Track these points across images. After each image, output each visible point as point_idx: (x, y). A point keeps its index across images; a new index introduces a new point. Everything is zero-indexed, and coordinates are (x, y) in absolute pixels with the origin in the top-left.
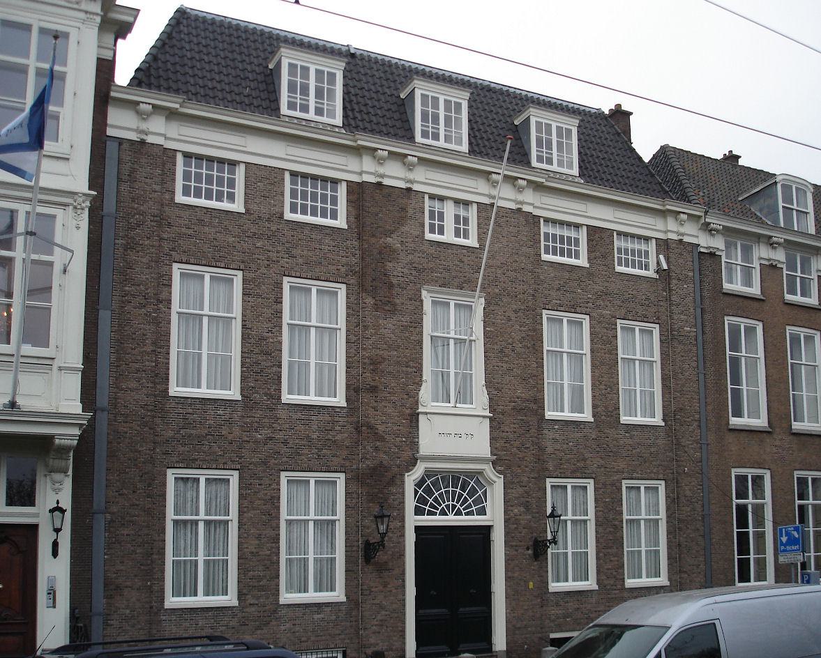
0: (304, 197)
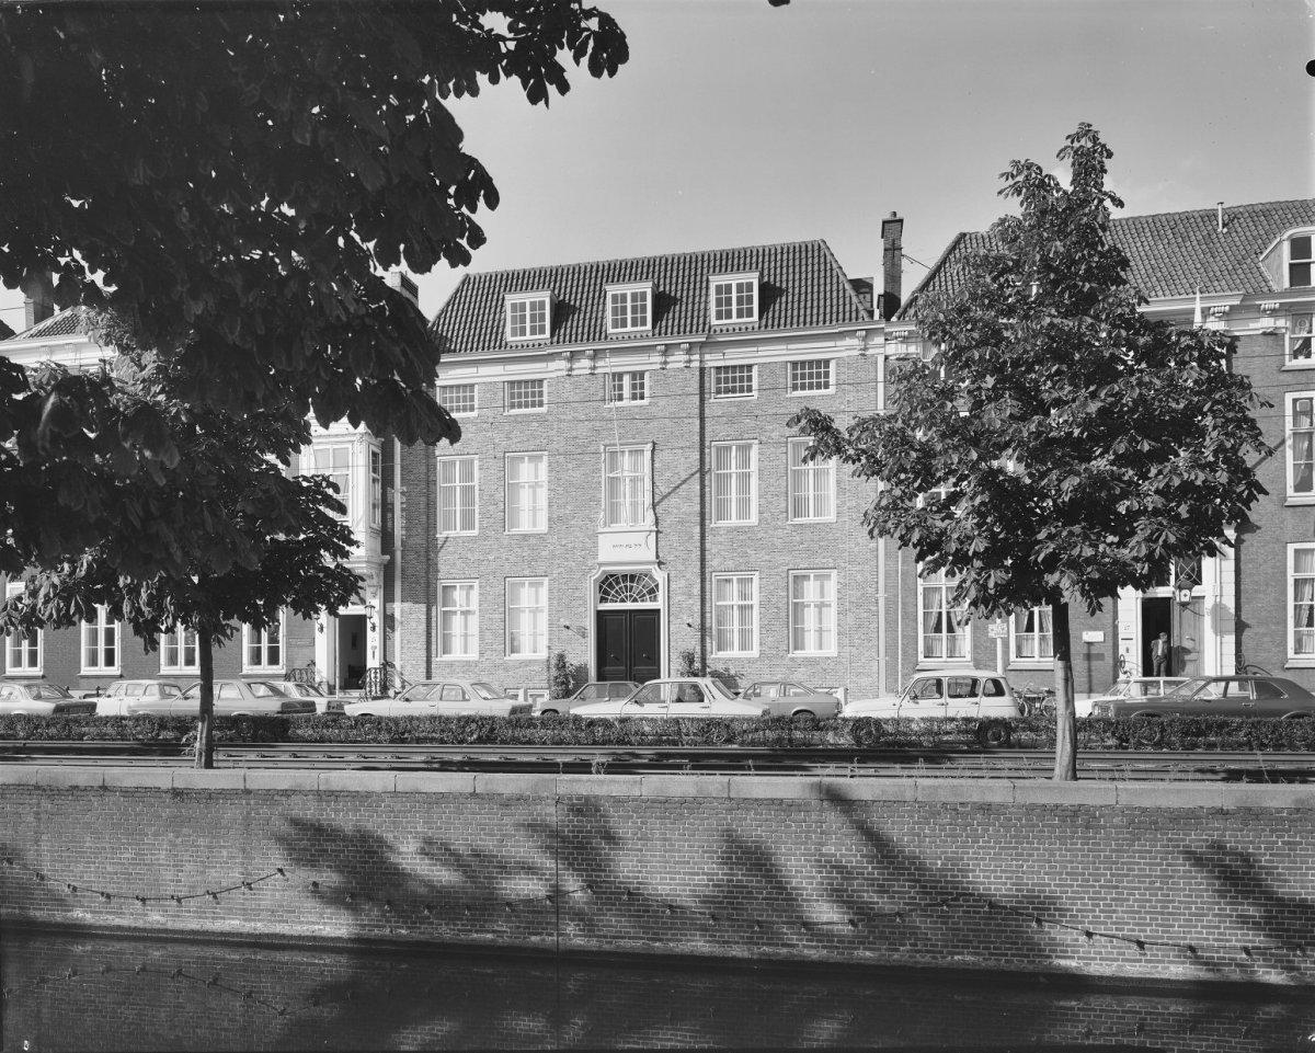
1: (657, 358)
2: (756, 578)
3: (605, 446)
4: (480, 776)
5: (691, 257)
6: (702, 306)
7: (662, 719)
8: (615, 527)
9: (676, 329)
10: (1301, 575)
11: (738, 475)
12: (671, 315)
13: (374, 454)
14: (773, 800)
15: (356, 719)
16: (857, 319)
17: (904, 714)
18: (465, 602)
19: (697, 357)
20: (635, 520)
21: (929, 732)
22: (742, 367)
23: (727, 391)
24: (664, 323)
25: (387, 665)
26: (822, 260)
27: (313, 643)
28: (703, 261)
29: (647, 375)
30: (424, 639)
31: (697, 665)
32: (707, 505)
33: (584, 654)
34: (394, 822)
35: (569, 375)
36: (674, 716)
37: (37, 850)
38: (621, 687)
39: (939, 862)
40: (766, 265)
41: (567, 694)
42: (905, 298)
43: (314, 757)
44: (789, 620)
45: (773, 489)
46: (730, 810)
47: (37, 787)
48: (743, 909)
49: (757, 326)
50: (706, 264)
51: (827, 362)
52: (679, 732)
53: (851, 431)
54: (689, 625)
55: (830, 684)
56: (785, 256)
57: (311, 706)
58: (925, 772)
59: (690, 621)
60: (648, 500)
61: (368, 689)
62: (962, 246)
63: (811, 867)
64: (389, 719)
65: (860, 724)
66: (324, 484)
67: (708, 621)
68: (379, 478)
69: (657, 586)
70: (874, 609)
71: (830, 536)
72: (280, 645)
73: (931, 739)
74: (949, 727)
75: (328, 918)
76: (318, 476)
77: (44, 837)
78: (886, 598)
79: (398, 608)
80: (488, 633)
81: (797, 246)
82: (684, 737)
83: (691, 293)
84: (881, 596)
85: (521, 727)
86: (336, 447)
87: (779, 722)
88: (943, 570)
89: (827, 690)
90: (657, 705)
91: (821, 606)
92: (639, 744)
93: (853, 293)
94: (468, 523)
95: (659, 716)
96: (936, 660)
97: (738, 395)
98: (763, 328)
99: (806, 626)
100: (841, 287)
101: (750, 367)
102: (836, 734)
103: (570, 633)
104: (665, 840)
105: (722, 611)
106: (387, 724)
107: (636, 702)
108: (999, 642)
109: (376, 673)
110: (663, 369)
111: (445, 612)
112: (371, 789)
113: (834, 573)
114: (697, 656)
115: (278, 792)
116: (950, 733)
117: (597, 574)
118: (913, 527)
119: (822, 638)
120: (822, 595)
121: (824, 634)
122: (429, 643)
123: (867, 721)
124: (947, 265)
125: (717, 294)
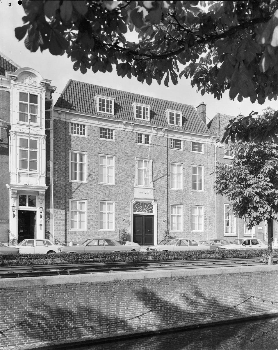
0: (174, 144)
8: (140, 186)
19: (166, 134)
35: (124, 130)
37: (261, 292)
44: (189, 220)
47: (261, 272)
77: (263, 288)
78: (217, 216)
79: (52, 210)
80: (91, 221)
86: (31, 139)
91: (109, 214)
110: (156, 135)
117: (134, 202)
122: (66, 224)
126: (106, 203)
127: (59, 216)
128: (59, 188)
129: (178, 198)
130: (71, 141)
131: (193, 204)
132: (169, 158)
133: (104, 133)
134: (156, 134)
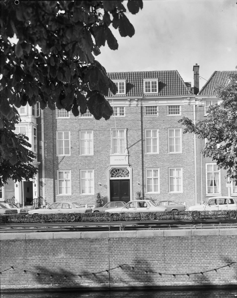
1: (128, 103)
2: (159, 170)
3: (112, 129)
4: (82, 232)
5: (137, 73)
6: (141, 88)
7: (135, 213)
8: (115, 154)
9: (133, 94)
10: (209, 172)
11: (65, 141)
12: (132, 90)
13: (35, 129)
14: (177, 237)
15: (33, 215)
16: (187, 94)
17: (207, 209)
18: (67, 177)
19: (140, 103)
20: (121, 152)
21: (214, 215)
22: (154, 106)
23: (149, 113)
24: (129, 92)
25: (40, 197)
26: (177, 76)
27: (14, 191)
28: (141, 74)
29: (125, 108)
30: (53, 189)
31: (141, 196)
32: (144, 148)
33: (106, 193)
34: (53, 249)
36: (139, 212)
38: (119, 203)
39: (226, 253)
40: (160, 77)
41: (101, 206)
42: (200, 88)
43: (19, 228)
44: (169, 183)
45: (163, 143)
46: (164, 240)
48: (168, 271)
49: (158, 94)
50: (142, 75)
51: (179, 106)
52: (140, 217)
53: (197, 125)
54: (139, 184)
55: (181, 201)
56: (166, 74)
57: (16, 211)
58: (221, 227)
59: (139, 183)
60: (126, 147)
61: (34, 205)
62: (216, 75)
63: (189, 256)
64: (44, 215)
65: (194, 213)
66: (23, 137)
67: (145, 183)
68: (36, 137)
69: (129, 172)
70: (193, 179)
71: (180, 158)
72: (2, 191)
73: (215, 217)
74: (219, 213)
75: (30, 282)
76: (21, 134)
79: (43, 180)
80: (74, 187)
81: (169, 71)
82: (142, 218)
83: (138, 84)
84: (195, 175)
85: (89, 216)
86: (21, 126)
87: (170, 213)
88: (223, 167)
89: (180, 203)
90: (133, 209)
92: (128, 221)
93: (186, 86)
94: (67, 152)
95: (134, 212)
96: (217, 193)
97: (155, 115)
98: (160, 95)
99: (62, 187)
100: (182, 85)
101: (156, 107)
102: (187, 216)
103: (101, 187)
104: (144, 250)
105: (149, 179)
106: (44, 217)
107: (126, 208)
108: (229, 188)
109: (36, 200)
110: (130, 106)
111: (60, 180)
112: (44, 238)
113: (182, 169)
114: (142, 193)
115: (11, 241)
116: (220, 215)
117: (110, 168)
118: (217, 154)
119: (179, 188)
120: (178, 175)
121: (179, 187)
123: (196, 212)
124: (212, 80)
125: (146, 84)
126: (175, 169)
127: (49, 184)
128: (48, 162)
129: (154, 161)
130: (57, 123)
131: (170, 166)
132: (144, 125)
133: (149, 110)
134: (129, 104)
